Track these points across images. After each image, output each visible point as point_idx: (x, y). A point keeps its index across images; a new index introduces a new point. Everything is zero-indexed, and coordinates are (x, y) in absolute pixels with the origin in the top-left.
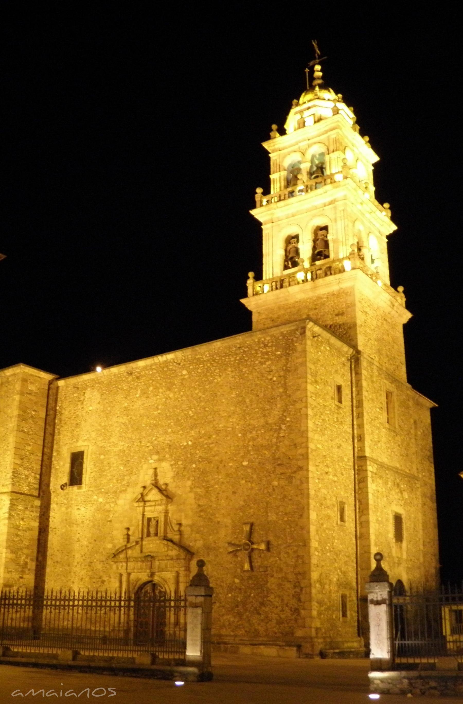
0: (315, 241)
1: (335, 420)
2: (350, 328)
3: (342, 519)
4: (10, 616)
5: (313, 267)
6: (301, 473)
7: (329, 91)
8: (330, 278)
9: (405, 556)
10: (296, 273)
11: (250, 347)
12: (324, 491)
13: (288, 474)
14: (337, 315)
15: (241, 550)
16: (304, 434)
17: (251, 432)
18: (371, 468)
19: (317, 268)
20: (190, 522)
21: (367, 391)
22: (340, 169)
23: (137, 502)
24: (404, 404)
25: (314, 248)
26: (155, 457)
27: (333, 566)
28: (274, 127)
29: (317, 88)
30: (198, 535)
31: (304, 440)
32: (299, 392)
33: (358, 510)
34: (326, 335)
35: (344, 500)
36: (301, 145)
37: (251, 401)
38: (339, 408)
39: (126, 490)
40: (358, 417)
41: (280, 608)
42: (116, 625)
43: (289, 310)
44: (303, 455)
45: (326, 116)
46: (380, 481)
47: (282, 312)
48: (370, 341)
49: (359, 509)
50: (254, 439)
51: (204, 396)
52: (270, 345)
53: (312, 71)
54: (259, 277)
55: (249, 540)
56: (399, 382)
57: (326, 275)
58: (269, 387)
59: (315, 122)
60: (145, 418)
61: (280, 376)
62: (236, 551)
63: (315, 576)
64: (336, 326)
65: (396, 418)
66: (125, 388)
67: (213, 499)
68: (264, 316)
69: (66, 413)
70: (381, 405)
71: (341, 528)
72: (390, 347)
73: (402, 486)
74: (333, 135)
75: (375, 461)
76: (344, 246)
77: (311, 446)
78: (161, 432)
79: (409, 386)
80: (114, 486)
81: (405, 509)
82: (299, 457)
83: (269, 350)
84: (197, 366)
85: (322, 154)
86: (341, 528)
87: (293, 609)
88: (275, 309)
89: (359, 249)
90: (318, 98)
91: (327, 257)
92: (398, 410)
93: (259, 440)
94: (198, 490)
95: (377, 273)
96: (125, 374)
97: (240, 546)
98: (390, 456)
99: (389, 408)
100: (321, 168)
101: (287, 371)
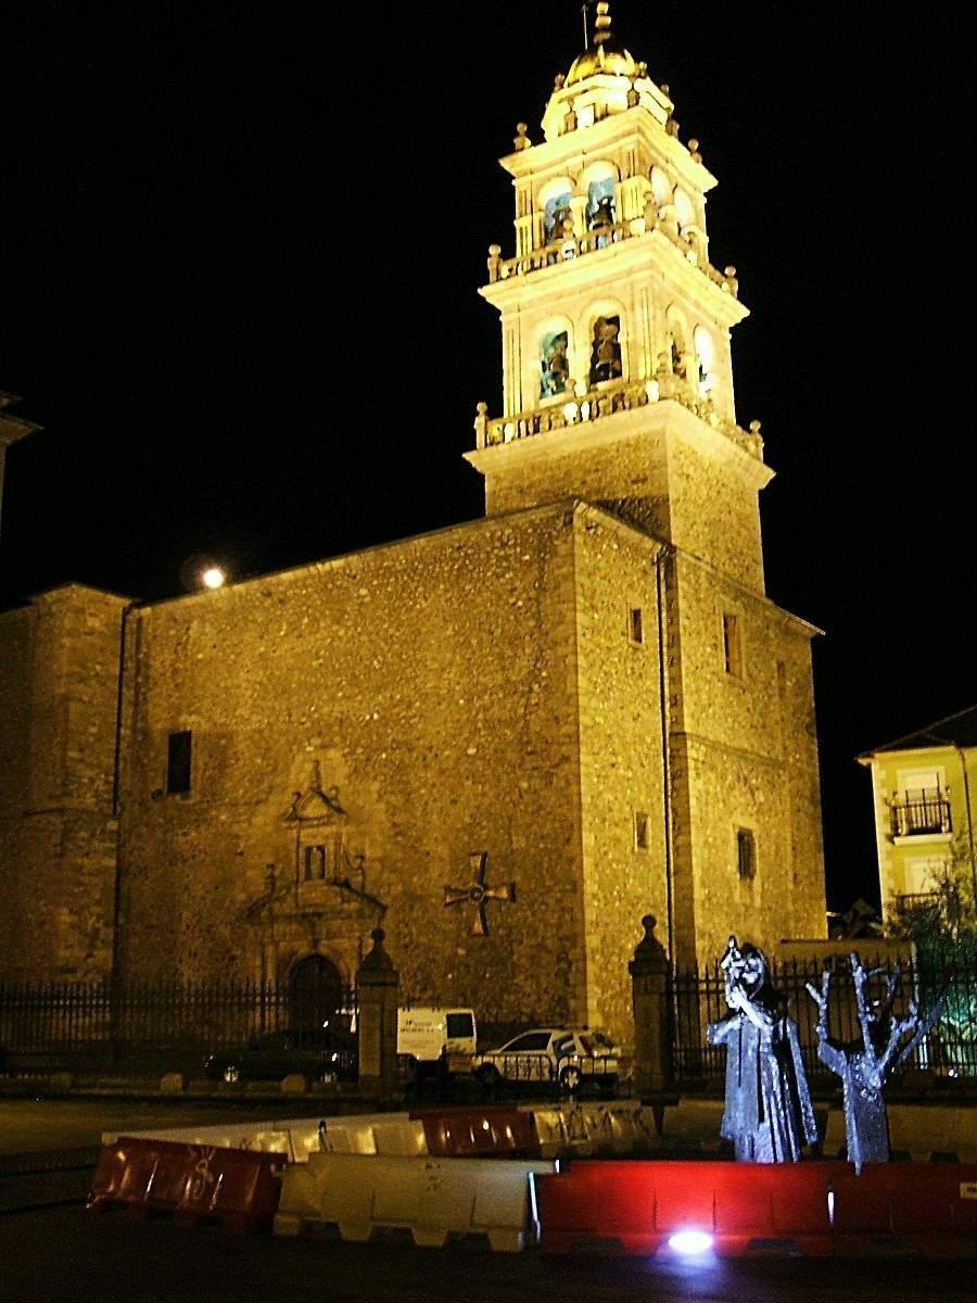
0: (595, 345)
1: (629, 672)
2: (657, 505)
3: (642, 842)
4: (74, 1022)
5: (592, 395)
6: (566, 766)
7: (623, 56)
8: (621, 416)
9: (758, 902)
10: (562, 404)
11: (477, 547)
12: (609, 796)
13: (545, 769)
14: (634, 482)
15: (467, 899)
16: (572, 699)
17: (480, 698)
18: (694, 752)
19: (599, 396)
20: (379, 853)
21: (688, 618)
22: (641, 213)
23: (286, 820)
24: (759, 636)
25: (594, 359)
26: (317, 741)
27: (627, 924)
28: (521, 128)
29: (601, 51)
30: (393, 876)
31: (571, 710)
32: (561, 628)
33: (671, 826)
34: (611, 523)
35: (645, 811)
36: (569, 163)
37: (480, 642)
38: (636, 650)
39: (267, 798)
40: (671, 664)
41: (534, 997)
42: (256, 1030)
43: (549, 473)
44: (570, 736)
45: (617, 108)
46: (712, 776)
47: (537, 476)
48: (695, 527)
49: (674, 823)
50: (485, 709)
51: (397, 634)
52: (511, 543)
53: (593, 15)
54: (495, 412)
55: (481, 883)
56: (749, 596)
57: (615, 409)
58: (512, 618)
59: (596, 120)
60: (296, 673)
61: (530, 599)
62: (459, 901)
63: (592, 941)
64: (632, 502)
65: (744, 661)
66: (259, 621)
67: (418, 813)
68: (505, 484)
69: (157, 664)
70: (714, 641)
71: (641, 859)
72: (734, 535)
73: (754, 781)
74: (629, 144)
75: (702, 740)
76: (648, 356)
77: (584, 719)
78: (325, 697)
79: (770, 602)
80: (246, 792)
81: (758, 821)
82: (562, 740)
83: (512, 552)
84: (385, 581)
85: (608, 183)
86: (641, 859)
87: (556, 998)
88: (525, 471)
89: (676, 359)
90: (602, 73)
91: (618, 374)
92: (747, 647)
93: (496, 709)
94: (393, 799)
95: (710, 401)
96: (259, 594)
97: (462, 892)
98: (732, 728)
99: (730, 646)
100: (606, 209)
101: (542, 590)
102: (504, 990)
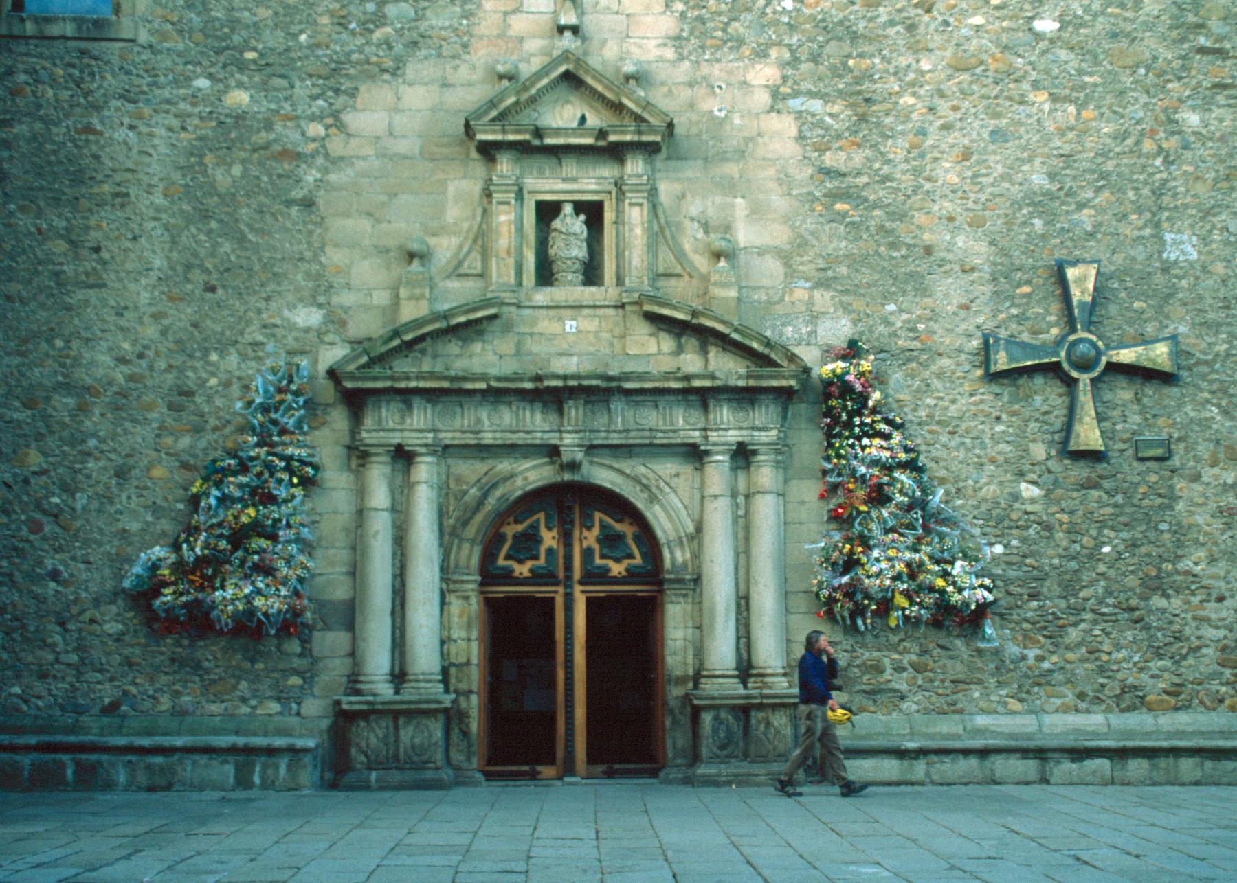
20: (778, 235)
102: (1156, 585)
